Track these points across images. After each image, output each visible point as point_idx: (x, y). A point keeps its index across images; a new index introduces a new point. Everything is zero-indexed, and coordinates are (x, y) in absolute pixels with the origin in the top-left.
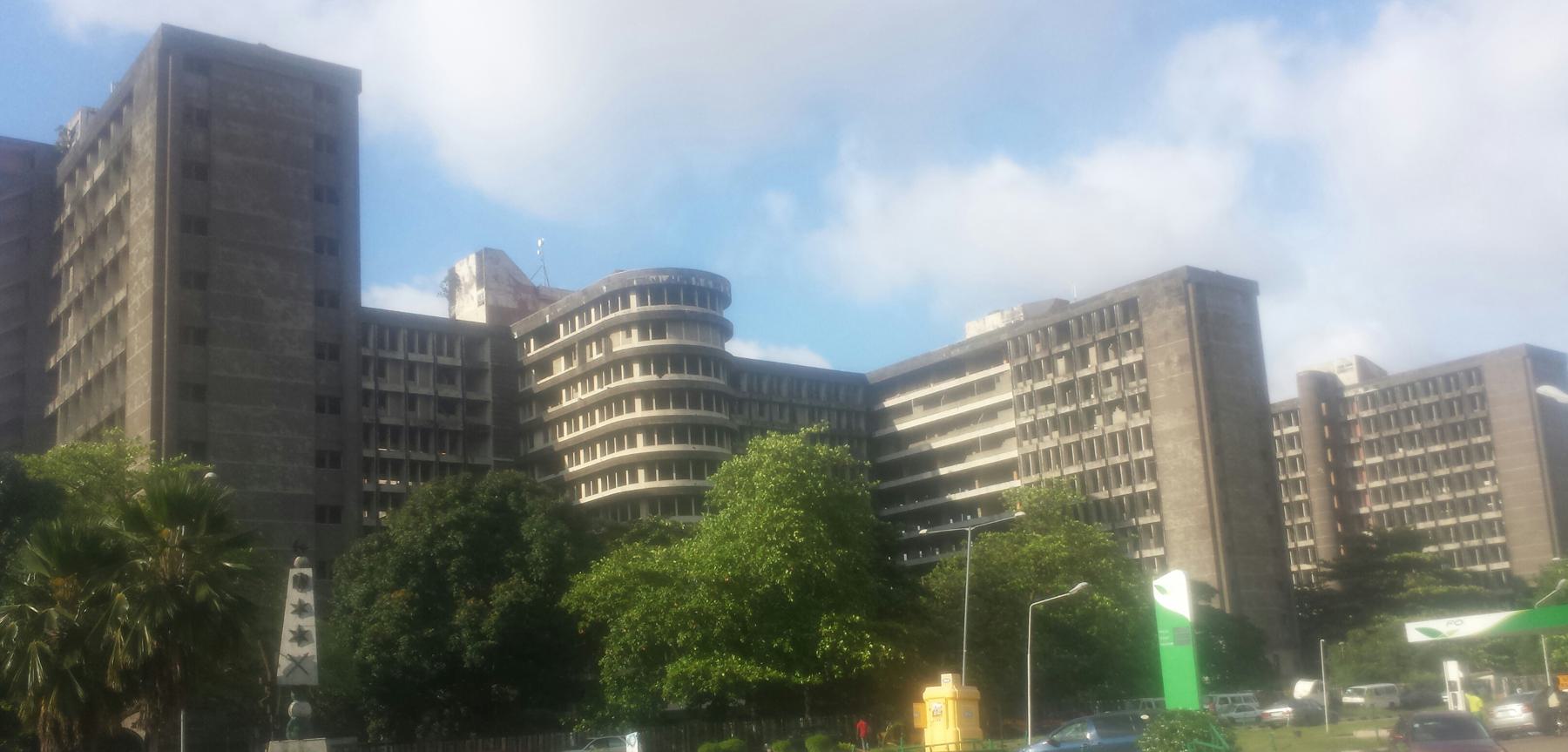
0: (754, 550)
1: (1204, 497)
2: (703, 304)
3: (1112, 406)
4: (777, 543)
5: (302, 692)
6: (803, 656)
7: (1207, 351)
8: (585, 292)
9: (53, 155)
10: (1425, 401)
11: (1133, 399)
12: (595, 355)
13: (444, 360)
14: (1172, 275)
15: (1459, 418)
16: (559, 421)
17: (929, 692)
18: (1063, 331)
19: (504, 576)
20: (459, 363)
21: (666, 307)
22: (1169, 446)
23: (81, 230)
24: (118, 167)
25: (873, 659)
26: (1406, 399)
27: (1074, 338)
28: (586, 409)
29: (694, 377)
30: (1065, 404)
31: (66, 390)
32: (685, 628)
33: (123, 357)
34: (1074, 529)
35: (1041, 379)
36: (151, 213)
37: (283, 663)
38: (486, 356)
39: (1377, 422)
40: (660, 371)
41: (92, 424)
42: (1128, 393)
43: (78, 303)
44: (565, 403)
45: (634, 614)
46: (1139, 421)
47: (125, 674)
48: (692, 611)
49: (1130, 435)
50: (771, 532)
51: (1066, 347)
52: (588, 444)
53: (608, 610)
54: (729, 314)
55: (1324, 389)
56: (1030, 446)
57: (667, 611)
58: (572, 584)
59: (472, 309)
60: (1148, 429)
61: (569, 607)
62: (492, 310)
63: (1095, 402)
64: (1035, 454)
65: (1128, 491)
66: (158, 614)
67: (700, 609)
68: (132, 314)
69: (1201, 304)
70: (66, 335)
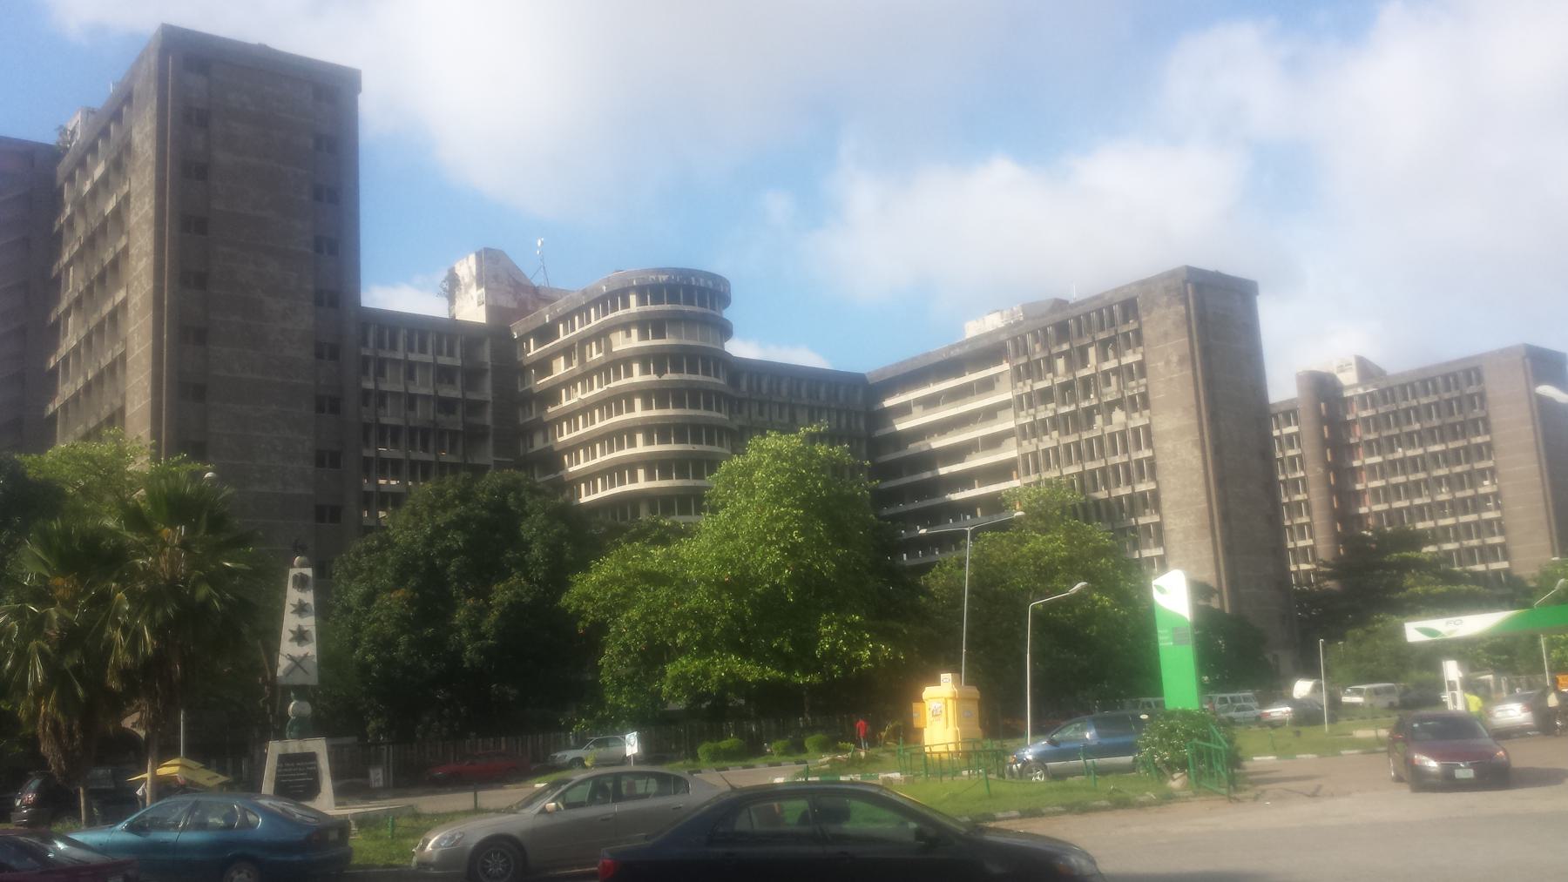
0: (753, 550)
1: (1203, 497)
2: (702, 304)
3: (1111, 406)
4: (777, 543)
5: (302, 691)
6: (803, 655)
7: (1207, 351)
8: (584, 292)
9: (53, 155)
10: (1424, 401)
11: (1132, 398)
12: (595, 355)
13: (444, 360)
14: (1173, 274)
15: (1458, 418)
16: (558, 420)
17: (929, 692)
18: (1062, 331)
19: (504, 575)
20: (459, 363)
21: (666, 307)
22: (1168, 446)
23: (81, 230)
24: (118, 166)
25: (872, 659)
26: (1406, 399)
27: (1073, 337)
28: (586, 409)
29: (693, 377)
30: (1064, 403)
31: (66, 390)
32: (684, 628)
33: (123, 357)
34: (1074, 529)
35: (1041, 379)
36: (151, 214)
37: (283, 663)
38: (486, 355)
39: (1377, 422)
40: (660, 371)
41: (92, 424)
42: (1128, 393)
43: (78, 302)
44: (565, 403)
45: (634, 613)
46: (1138, 421)
47: (125, 674)
48: (692, 610)
49: (1130, 436)
50: (771, 531)
51: (1065, 347)
52: (587, 443)
53: (607, 610)
54: (728, 314)
55: (1323, 388)
56: (1029, 446)
57: (666, 611)
58: (571, 584)
59: (472, 309)
60: (1147, 428)
61: (569, 606)
62: (492, 310)
63: (1095, 402)
64: (1035, 454)
65: (1128, 491)
66: (158, 614)
67: (700, 609)
68: (132, 313)
69: (1201, 306)
70: (66, 335)
